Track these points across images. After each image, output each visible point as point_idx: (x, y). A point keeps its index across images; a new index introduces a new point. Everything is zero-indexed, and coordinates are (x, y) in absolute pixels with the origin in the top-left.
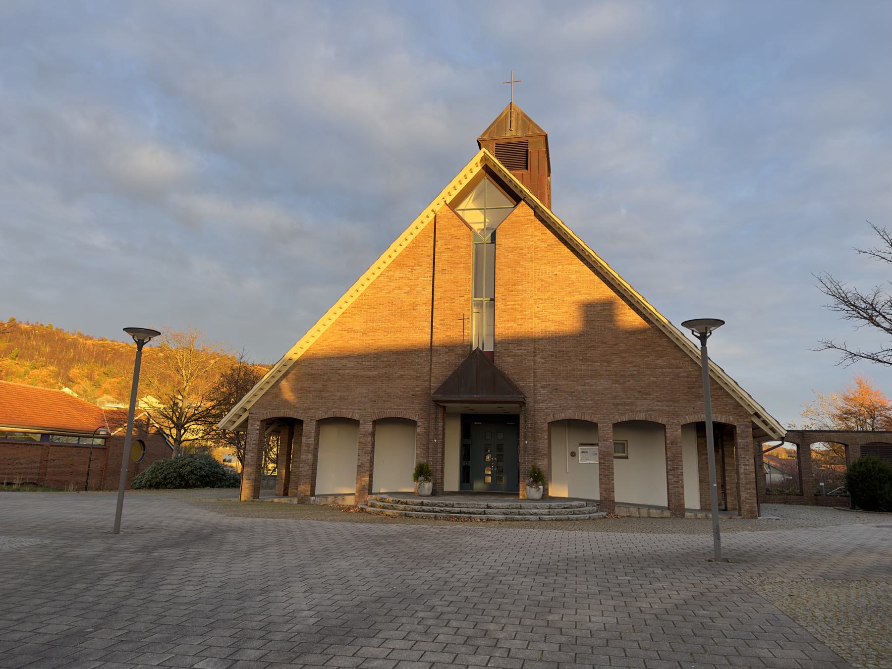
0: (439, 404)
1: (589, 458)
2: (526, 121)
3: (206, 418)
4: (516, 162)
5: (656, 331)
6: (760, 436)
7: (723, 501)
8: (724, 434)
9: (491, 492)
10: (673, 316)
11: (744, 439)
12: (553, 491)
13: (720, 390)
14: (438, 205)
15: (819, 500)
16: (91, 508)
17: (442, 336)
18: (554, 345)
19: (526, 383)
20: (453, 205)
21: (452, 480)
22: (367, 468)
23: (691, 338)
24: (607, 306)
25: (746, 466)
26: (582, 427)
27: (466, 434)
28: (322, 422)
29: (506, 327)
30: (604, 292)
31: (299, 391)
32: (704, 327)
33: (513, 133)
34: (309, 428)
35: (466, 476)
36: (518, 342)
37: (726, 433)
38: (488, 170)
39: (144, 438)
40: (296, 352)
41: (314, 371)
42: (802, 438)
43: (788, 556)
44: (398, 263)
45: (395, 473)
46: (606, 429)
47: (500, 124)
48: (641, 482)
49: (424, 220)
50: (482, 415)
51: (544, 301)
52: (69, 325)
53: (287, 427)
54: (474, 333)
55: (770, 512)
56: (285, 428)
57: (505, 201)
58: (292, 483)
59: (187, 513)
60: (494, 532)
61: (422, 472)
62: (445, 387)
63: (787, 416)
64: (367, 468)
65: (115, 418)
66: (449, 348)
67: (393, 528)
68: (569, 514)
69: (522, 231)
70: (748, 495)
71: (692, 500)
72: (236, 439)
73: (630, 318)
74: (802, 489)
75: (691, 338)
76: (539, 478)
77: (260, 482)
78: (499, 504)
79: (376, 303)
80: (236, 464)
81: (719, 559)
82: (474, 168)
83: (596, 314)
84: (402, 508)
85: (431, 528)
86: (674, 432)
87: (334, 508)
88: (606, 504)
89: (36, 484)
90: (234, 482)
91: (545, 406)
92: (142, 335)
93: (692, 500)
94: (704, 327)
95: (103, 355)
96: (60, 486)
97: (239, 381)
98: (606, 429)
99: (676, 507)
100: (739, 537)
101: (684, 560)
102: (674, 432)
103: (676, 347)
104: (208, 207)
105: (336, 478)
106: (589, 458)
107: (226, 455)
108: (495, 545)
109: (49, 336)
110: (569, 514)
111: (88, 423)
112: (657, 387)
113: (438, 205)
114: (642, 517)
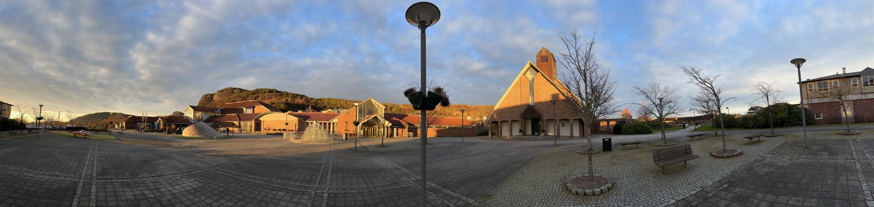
2: (547, 51)
14: (521, 74)
19: (541, 112)
22: (511, 131)
28: (502, 122)
29: (537, 100)
30: (557, 92)
33: (544, 54)
36: (539, 103)
40: (496, 108)
41: (500, 112)
47: (541, 52)
50: (532, 118)
53: (496, 123)
59: (58, 176)
61: (520, 131)
64: (511, 131)
66: (525, 105)
79: (511, 96)
81: (556, 145)
82: (528, 65)
87: (505, 139)
91: (545, 116)
104: (490, 73)
105: (505, 133)
110: (551, 138)
113: (521, 74)
114: (565, 138)
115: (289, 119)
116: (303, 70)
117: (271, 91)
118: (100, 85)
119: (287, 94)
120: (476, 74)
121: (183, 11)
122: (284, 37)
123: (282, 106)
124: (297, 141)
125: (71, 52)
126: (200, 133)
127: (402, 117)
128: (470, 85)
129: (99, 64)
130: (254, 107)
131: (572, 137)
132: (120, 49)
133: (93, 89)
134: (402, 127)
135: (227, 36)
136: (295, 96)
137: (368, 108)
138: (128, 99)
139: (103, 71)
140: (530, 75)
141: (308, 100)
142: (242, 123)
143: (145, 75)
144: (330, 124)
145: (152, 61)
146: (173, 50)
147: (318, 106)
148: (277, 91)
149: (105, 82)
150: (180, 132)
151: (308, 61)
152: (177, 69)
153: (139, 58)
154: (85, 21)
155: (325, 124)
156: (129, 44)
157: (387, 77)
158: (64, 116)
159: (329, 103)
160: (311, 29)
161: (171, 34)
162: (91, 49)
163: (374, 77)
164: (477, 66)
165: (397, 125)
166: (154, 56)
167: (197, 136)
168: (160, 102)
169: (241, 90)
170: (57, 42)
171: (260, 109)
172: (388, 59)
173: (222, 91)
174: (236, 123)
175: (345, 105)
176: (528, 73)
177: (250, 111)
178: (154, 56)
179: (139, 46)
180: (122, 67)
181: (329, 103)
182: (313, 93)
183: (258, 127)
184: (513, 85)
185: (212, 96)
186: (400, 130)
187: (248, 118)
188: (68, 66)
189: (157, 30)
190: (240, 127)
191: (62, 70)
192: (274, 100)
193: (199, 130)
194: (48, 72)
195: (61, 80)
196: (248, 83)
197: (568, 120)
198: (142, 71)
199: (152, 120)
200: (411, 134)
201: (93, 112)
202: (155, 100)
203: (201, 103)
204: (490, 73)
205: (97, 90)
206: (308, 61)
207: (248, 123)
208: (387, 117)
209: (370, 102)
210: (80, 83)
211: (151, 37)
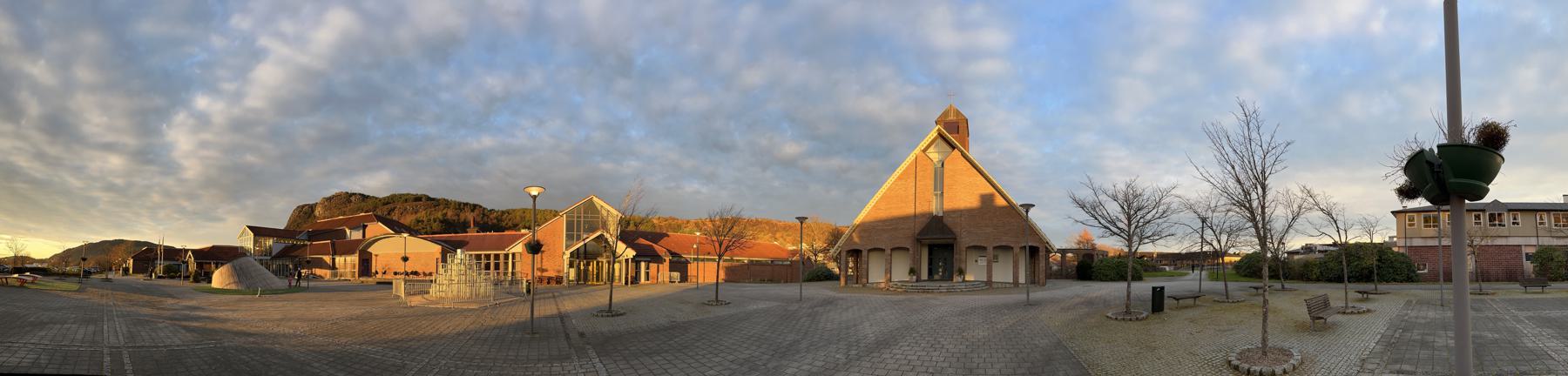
0: (919, 241)
1: (983, 262)
2: (958, 113)
3: (825, 251)
4: (954, 131)
5: (1011, 205)
6: (1048, 251)
7: (1033, 280)
8: (1034, 252)
9: (942, 280)
10: (1017, 201)
11: (1042, 253)
12: (968, 278)
13: (1032, 230)
14: (917, 151)
15: (1068, 277)
16: (790, 290)
17: (919, 210)
18: (969, 213)
19: (957, 230)
20: (924, 151)
21: (925, 275)
22: (889, 271)
23: (1023, 211)
24: (992, 195)
25: (1042, 264)
26: (980, 249)
27: (930, 254)
29: (948, 205)
31: (860, 237)
32: (1028, 207)
33: (952, 118)
34: (864, 253)
35: (930, 273)
36: (954, 211)
37: (1036, 250)
38: (941, 135)
39: (806, 262)
40: (860, 218)
41: (866, 229)
42: (1063, 252)
43: (1052, 301)
44: (899, 178)
45: (901, 273)
46: (990, 249)
47: (946, 114)
48: (1002, 273)
49: (912, 157)
50: (937, 244)
51: (964, 194)
52: (773, 218)
53: (856, 253)
54: (934, 207)
55: (1050, 283)
56: (857, 251)
57: (948, 149)
58: (859, 277)
60: (943, 297)
61: (912, 271)
62: (922, 232)
63: (1058, 244)
64: (889, 271)
65: (794, 253)
66: (923, 215)
67: (902, 297)
68: (974, 288)
69: (955, 161)
70: (1042, 276)
71: (1022, 280)
72: (836, 260)
73: (1000, 201)
74: (1063, 274)
75: (1023, 211)
76: (961, 272)
77: (847, 278)
78: (944, 284)
79: (892, 195)
80: (837, 270)
81: (1029, 304)
82: (934, 134)
83: (987, 200)
84: (903, 288)
85: (916, 297)
86: (1017, 250)
87: (876, 289)
88: (989, 283)
89: (771, 281)
90: (837, 278)
91: (965, 240)
92: (802, 220)
93: (1022, 280)
94: (1028, 207)
95: (787, 228)
96: (778, 282)
97: (836, 235)
98: (990, 249)
99: (1016, 283)
100: (1038, 294)
101: (1008, 307)
102: (1017, 250)
103: (1019, 215)
104: (813, 163)
105: (876, 275)
106: (983, 262)
107: (833, 267)
108: (944, 303)
109: (768, 223)
110: (974, 288)
111: (784, 255)
112: (1008, 228)
113: (917, 151)
114: (1004, 287)
115: (424, 250)
116: (477, 158)
117: (418, 198)
118: (111, 188)
119: (447, 203)
120: (789, 163)
121: (257, 55)
122: (445, 96)
123: (435, 226)
124: (416, 301)
125: (59, 126)
126: (239, 282)
127: (657, 237)
128: (776, 184)
129: (109, 147)
130: (365, 227)
131: (1016, 283)
132: (148, 123)
133: (96, 194)
134: (656, 258)
135: (344, 97)
136: (461, 206)
137: (585, 219)
138: (162, 214)
139: (115, 161)
140: (934, 155)
141: (485, 213)
142: (338, 259)
143: (192, 169)
144: (506, 256)
145: (204, 145)
146: (239, 125)
147: (496, 223)
148: (429, 199)
149: (119, 181)
150: (208, 278)
151: (487, 141)
152: (250, 158)
153: (180, 139)
154: (84, 73)
155: (497, 257)
156: (164, 114)
157: (632, 165)
158: (42, 247)
159: (523, 218)
160: (493, 82)
161: (238, 97)
162: (95, 118)
163: (607, 166)
164: (790, 149)
165: (646, 255)
166: (207, 136)
167: (234, 287)
168: (220, 220)
169: (364, 197)
170: (34, 108)
171: (376, 228)
172: (633, 133)
173: (330, 199)
174: (327, 259)
175: (533, 217)
176: (931, 149)
177: (356, 235)
178: (207, 136)
179: (181, 117)
180: (149, 156)
181: (523, 218)
182: (494, 201)
183: (365, 266)
184: (899, 171)
185: (312, 207)
186: (653, 266)
187: (349, 248)
188: (53, 151)
189: (212, 89)
190: (333, 267)
191: (40, 156)
192: (422, 215)
193: (240, 274)
194: (13, 158)
195: (38, 175)
196: (376, 184)
197: (984, 248)
198: (186, 163)
199: (171, 253)
200: (676, 275)
201: (111, 236)
202: (209, 216)
203: (292, 221)
204: (813, 163)
205: (105, 197)
206: (487, 141)
207: (349, 258)
208: (626, 237)
209: (590, 207)
210: (74, 182)
211: (202, 102)
